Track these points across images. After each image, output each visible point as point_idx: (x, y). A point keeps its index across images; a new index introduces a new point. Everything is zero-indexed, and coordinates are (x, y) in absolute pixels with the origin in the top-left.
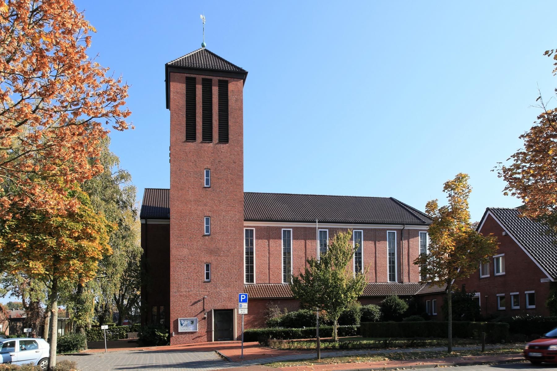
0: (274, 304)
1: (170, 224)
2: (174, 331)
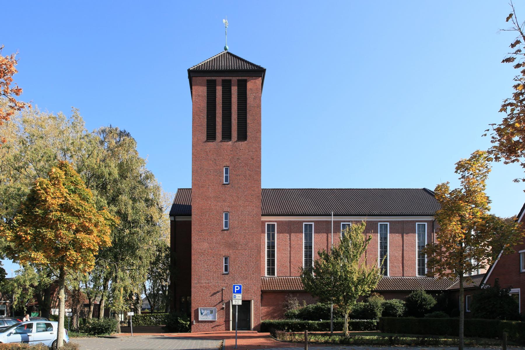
0: (293, 297)
1: (191, 221)
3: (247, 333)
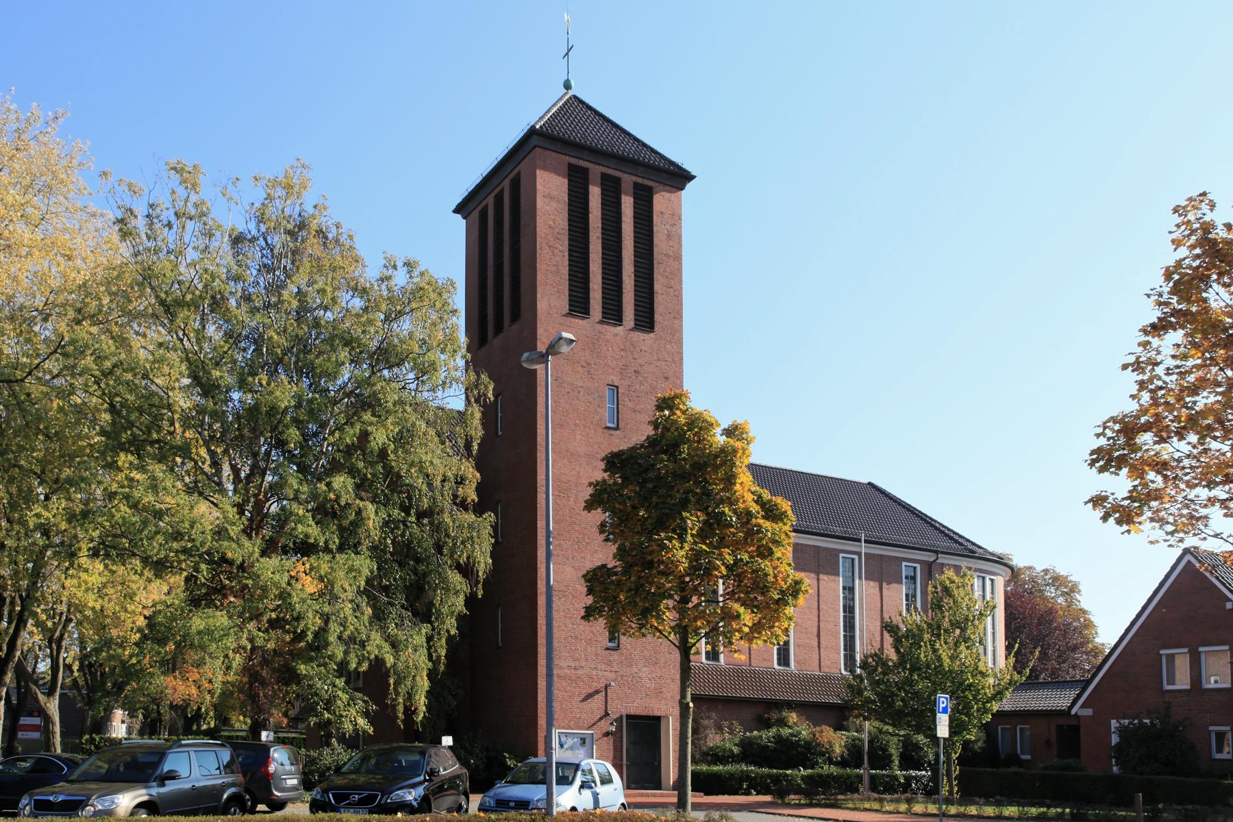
3: (654, 795)
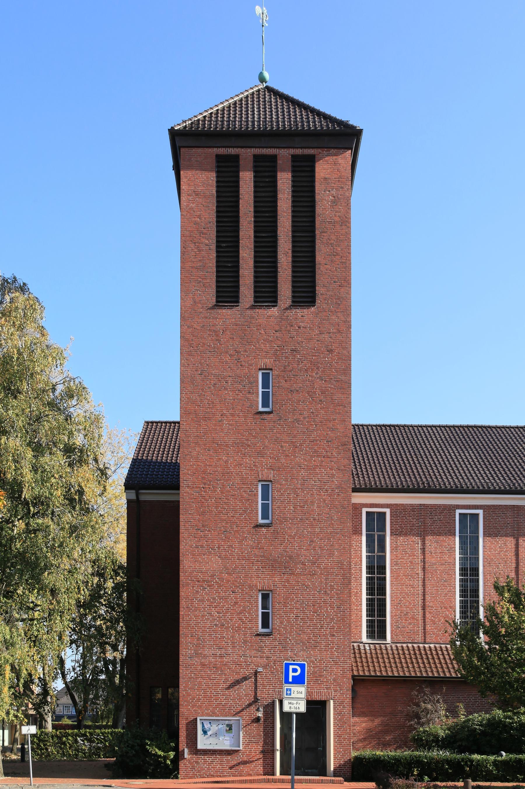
0: (432, 694)
1: (179, 502)
2: (188, 747)
